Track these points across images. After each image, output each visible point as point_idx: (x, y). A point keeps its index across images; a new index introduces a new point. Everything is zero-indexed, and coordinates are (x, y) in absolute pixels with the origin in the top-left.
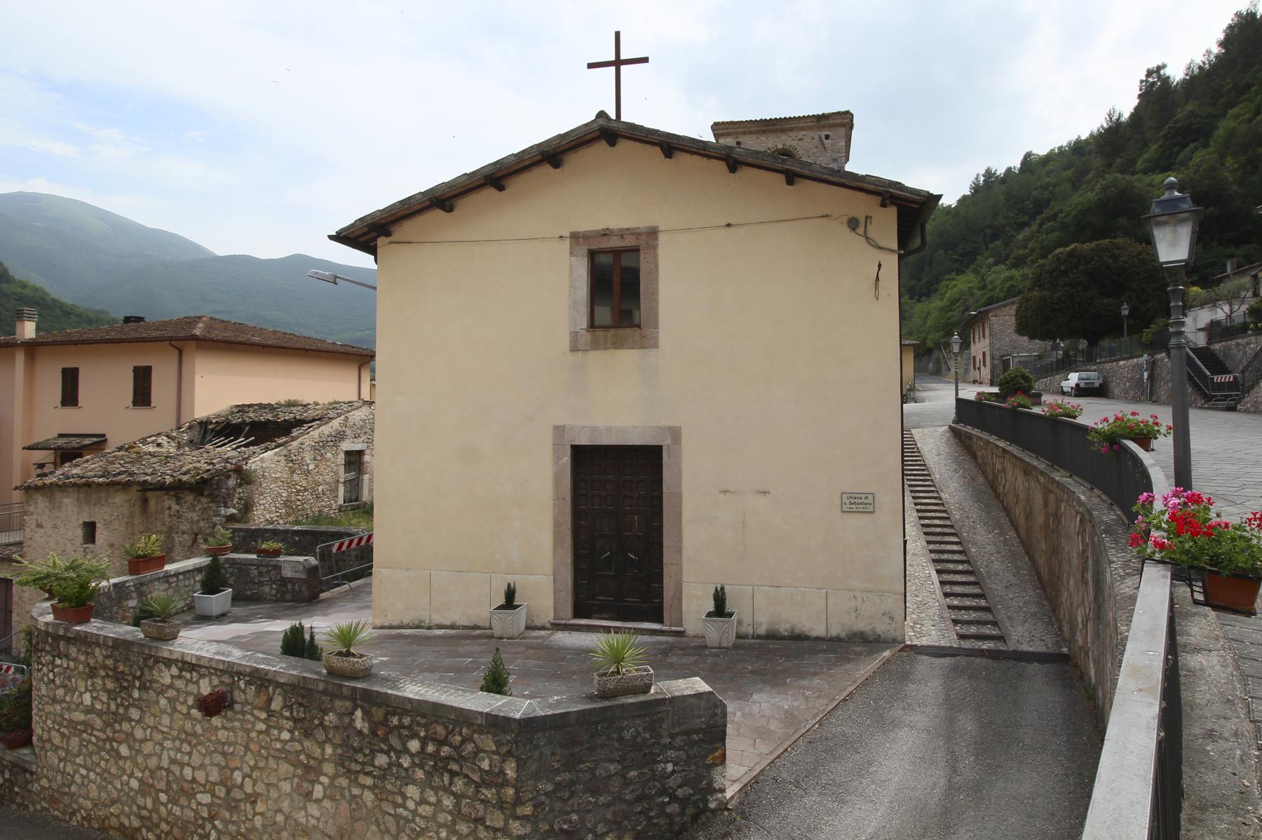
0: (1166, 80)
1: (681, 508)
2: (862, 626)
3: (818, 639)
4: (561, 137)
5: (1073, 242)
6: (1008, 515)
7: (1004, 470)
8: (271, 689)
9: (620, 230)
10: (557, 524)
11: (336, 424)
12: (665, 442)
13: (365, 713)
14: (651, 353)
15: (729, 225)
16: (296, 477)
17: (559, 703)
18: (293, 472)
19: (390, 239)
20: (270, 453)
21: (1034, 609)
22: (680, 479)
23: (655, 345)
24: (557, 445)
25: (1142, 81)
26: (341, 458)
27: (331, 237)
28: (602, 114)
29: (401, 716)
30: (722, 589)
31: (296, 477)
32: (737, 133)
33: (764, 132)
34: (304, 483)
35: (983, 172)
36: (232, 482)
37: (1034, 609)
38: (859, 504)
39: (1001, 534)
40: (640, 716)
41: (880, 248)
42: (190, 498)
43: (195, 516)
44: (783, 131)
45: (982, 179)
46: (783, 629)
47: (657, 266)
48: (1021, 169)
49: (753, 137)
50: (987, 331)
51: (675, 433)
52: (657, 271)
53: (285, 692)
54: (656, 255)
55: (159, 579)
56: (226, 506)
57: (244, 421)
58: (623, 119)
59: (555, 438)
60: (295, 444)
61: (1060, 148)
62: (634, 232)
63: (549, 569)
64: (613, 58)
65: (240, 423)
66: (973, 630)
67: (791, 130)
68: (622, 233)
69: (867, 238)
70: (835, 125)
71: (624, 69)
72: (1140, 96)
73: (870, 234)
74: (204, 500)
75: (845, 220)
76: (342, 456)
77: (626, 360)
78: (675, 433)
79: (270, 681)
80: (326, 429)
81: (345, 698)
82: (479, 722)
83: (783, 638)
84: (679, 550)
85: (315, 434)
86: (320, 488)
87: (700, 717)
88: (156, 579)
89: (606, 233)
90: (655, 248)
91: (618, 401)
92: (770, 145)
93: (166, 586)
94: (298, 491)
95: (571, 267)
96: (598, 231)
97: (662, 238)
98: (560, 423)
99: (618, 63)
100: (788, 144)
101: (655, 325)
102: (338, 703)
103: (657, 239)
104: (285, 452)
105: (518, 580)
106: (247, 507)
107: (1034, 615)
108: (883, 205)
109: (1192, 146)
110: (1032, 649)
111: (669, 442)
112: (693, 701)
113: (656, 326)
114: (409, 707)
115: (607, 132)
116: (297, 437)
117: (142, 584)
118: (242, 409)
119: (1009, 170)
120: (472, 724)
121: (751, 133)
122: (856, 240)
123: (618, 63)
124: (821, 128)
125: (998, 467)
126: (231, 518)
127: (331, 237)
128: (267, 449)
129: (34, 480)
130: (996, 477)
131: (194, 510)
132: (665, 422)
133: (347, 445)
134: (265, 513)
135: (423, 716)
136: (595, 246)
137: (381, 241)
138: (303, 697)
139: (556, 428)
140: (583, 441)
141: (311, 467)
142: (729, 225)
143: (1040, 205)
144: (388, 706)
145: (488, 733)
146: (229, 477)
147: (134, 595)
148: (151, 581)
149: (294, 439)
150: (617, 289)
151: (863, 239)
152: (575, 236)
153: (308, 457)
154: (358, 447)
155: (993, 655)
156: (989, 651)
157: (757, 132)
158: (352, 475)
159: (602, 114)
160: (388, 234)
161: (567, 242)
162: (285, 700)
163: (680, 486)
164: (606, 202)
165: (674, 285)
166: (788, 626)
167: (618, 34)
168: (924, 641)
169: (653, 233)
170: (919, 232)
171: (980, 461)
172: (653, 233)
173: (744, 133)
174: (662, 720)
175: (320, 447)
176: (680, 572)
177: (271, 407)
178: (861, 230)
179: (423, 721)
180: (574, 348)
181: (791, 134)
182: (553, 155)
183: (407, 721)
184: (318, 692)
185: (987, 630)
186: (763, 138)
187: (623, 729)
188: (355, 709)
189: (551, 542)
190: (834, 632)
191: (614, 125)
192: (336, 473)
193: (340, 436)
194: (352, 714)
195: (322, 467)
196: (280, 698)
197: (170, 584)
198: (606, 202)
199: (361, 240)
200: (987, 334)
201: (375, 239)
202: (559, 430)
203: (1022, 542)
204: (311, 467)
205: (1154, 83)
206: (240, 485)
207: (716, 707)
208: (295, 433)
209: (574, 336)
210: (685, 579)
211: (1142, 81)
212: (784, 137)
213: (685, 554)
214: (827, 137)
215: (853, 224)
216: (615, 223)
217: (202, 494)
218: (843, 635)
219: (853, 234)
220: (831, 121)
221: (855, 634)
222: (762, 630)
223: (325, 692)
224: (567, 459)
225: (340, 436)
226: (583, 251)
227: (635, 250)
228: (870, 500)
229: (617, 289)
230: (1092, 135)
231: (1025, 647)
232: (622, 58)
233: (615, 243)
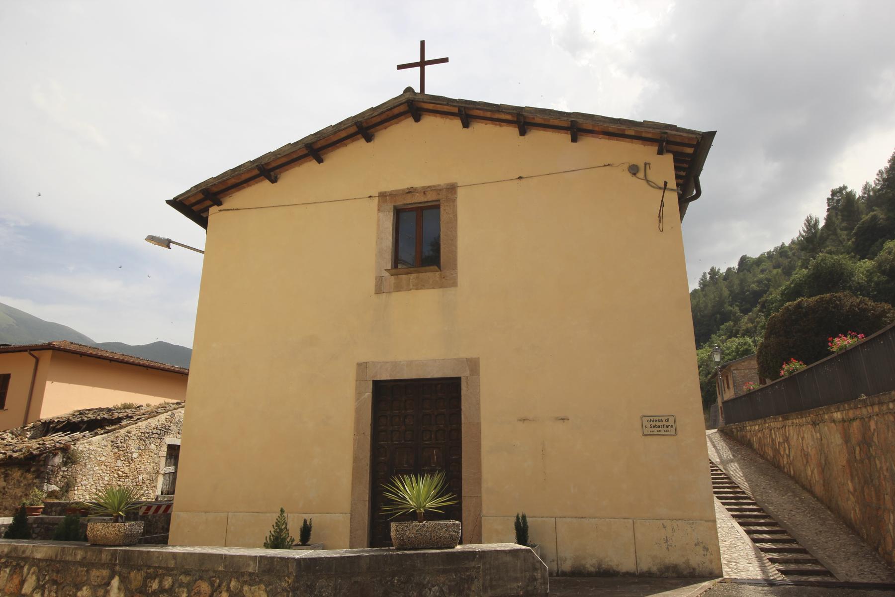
0: (850, 196)
1: (480, 438)
2: (674, 558)
3: (627, 574)
4: (373, 109)
5: (799, 297)
6: (797, 482)
7: (787, 440)
8: (25, 570)
9: (423, 187)
10: (356, 459)
11: (163, 417)
12: (464, 374)
13: (123, 580)
14: (451, 291)
15: (520, 178)
16: (119, 463)
17: (346, 552)
18: (118, 458)
19: (221, 208)
20: (98, 437)
21: (852, 549)
22: (478, 409)
23: (455, 284)
24: (360, 380)
25: (828, 199)
26: (164, 451)
27: (168, 202)
28: (409, 90)
29: (161, 577)
30: (524, 517)
31: (119, 463)
34: (126, 470)
35: (708, 270)
36: (58, 460)
37: (852, 549)
38: (660, 426)
39: (795, 495)
40: (445, 571)
42: (16, 474)
43: (19, 492)
45: (708, 276)
46: (590, 564)
47: (456, 216)
48: (739, 269)
50: (731, 382)
51: (473, 365)
53: (40, 570)
54: (455, 207)
56: (49, 482)
57: (82, 420)
59: (358, 374)
60: (123, 431)
61: (769, 253)
63: (346, 506)
64: (419, 60)
65: (79, 422)
66: (793, 567)
68: (425, 191)
69: (648, 181)
71: (427, 67)
72: (828, 210)
73: (650, 178)
74: (30, 476)
75: (627, 166)
76: (165, 448)
78: (473, 365)
79: (26, 559)
80: (153, 422)
81: (103, 566)
82: (251, 570)
83: (590, 575)
84: (478, 481)
85: (142, 424)
86: (141, 477)
87: (516, 580)
89: (410, 191)
90: (454, 201)
91: (418, 336)
94: (119, 477)
95: (379, 220)
96: (403, 190)
97: (461, 193)
98: (363, 359)
99: (422, 64)
101: (454, 265)
102: (94, 573)
103: (455, 193)
104: (112, 438)
105: (316, 519)
106: (68, 487)
107: (856, 554)
108: (660, 152)
109: (880, 240)
110: (865, 581)
111: (468, 373)
112: (508, 559)
114: (172, 564)
115: (413, 106)
116: (127, 426)
118: (81, 413)
119: (729, 269)
120: (243, 574)
122: (637, 183)
123: (422, 64)
125: (779, 439)
126: (52, 494)
127: (168, 202)
128: (96, 434)
130: (776, 451)
131: (19, 487)
132: (464, 354)
133: (170, 440)
134: (84, 493)
135: (187, 573)
136: (400, 202)
137: (213, 210)
138: (58, 572)
139: (359, 365)
140: (384, 376)
141: (135, 455)
142: (520, 178)
143: (757, 295)
144: (149, 567)
145: (261, 582)
146: (55, 455)
149: (121, 427)
150: (419, 239)
151: (644, 182)
152: (382, 196)
153: (133, 445)
154: (177, 442)
155: (827, 585)
156: (818, 582)
158: (171, 469)
159: (409, 90)
160: (219, 203)
161: (376, 200)
162: (38, 580)
163: (479, 418)
164: (409, 162)
165: (471, 234)
166: (594, 561)
168: (744, 575)
169: (452, 188)
170: (694, 185)
171: (756, 446)
172: (452, 188)
174: (470, 580)
175: (145, 438)
176: (479, 505)
177: (109, 410)
178: (641, 174)
179: (184, 579)
180: (379, 291)
182: (364, 127)
183: (168, 582)
184: (75, 563)
185: (809, 567)
187: (425, 586)
188: (112, 577)
189: (351, 478)
190: (644, 567)
191: (420, 97)
192: (157, 464)
193: (165, 430)
194: (108, 584)
195: (145, 457)
196: (34, 578)
198: (409, 162)
199: (194, 208)
200: (731, 386)
201: (207, 210)
202: (362, 367)
203: (819, 500)
204: (135, 455)
205: (838, 201)
206: (65, 464)
207: (535, 569)
208: (124, 423)
209: (380, 280)
210: (484, 512)
211: (828, 199)
213: (484, 485)
215: (634, 170)
216: (418, 182)
217: (28, 471)
218: (654, 569)
219: (634, 178)
221: (667, 568)
222: (567, 566)
223: (81, 563)
224: (368, 395)
225: (165, 430)
226: (390, 207)
227: (435, 207)
228: (671, 423)
229: (419, 239)
230: (793, 242)
231: (856, 579)
232: (426, 59)
233: (419, 198)
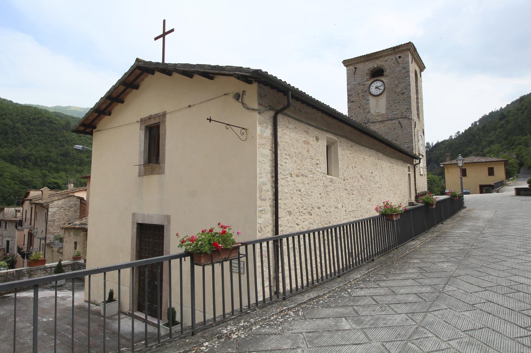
12: (165, 224)
23: (163, 173)
32: (355, 64)
33: (368, 60)
41: (248, 109)
44: (377, 58)
47: (165, 131)
49: (362, 64)
52: (165, 134)
55: (41, 269)
58: (165, 62)
62: (157, 116)
67: (381, 57)
70: (403, 51)
77: (155, 178)
88: (39, 269)
89: (150, 118)
92: (371, 67)
93: (45, 272)
97: (168, 116)
100: (379, 64)
113: (164, 163)
117: (31, 271)
121: (361, 62)
124: (396, 53)
129: (67, 226)
140: (147, 221)
142: (190, 106)
147: (27, 275)
148: (36, 270)
157: (364, 61)
167: (164, 21)
169: (164, 114)
172: (164, 114)
173: (358, 63)
178: (240, 100)
180: (140, 176)
181: (381, 59)
186: (367, 64)
197: (47, 271)
212: (377, 61)
214: (400, 57)
215: (237, 97)
220: (401, 49)
